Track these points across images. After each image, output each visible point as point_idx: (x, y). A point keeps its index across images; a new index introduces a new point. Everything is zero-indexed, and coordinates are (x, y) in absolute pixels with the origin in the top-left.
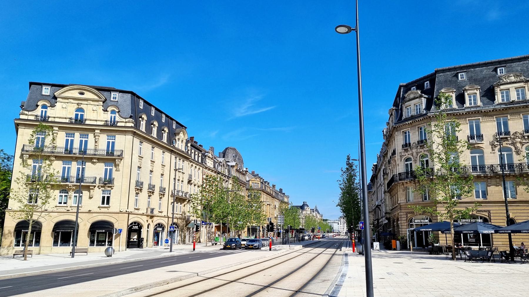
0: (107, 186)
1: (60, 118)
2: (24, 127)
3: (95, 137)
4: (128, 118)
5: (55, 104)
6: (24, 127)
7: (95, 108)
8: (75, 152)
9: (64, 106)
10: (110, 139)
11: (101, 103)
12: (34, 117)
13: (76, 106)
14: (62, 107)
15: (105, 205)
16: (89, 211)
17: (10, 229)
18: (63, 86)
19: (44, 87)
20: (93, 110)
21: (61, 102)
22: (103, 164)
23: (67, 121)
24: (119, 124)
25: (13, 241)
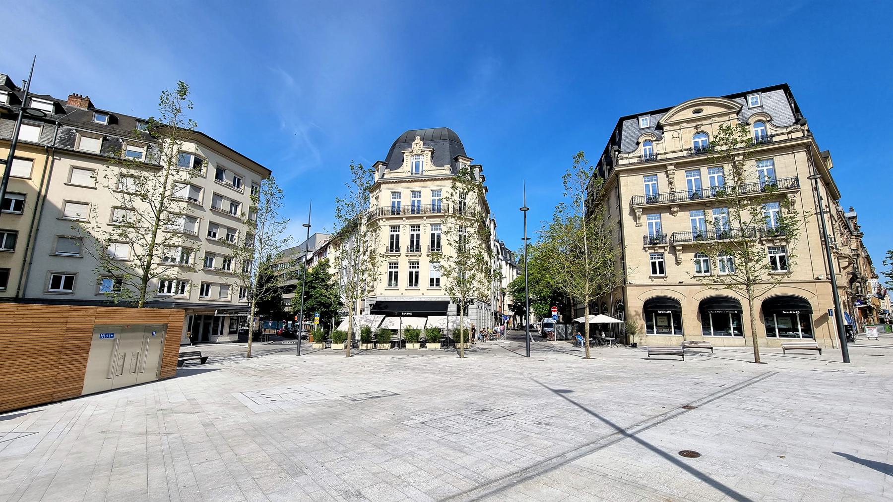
0: (657, 247)
1: (673, 152)
3: (668, 176)
4: (792, 125)
5: (662, 136)
7: (676, 135)
8: (786, 186)
9: (676, 135)
12: (637, 159)
13: (694, 131)
18: (666, 110)
19: (640, 119)
21: (670, 131)
25: (643, 326)
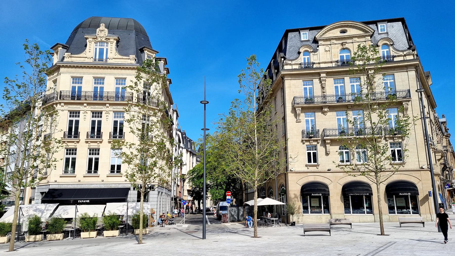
1: (325, 63)
2: (290, 79)
3: (321, 82)
6: (290, 79)
7: (327, 49)
9: (327, 49)
10: (387, 80)
11: (369, 38)
12: (298, 66)
13: (340, 47)
14: (324, 50)
15: (397, 161)
16: (328, 170)
17: (296, 193)
18: (321, 28)
20: (326, 51)
22: (335, 113)
23: (334, 65)
24: (396, 59)
25: (301, 206)
